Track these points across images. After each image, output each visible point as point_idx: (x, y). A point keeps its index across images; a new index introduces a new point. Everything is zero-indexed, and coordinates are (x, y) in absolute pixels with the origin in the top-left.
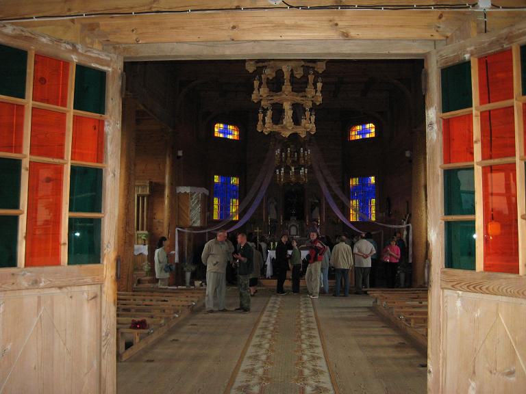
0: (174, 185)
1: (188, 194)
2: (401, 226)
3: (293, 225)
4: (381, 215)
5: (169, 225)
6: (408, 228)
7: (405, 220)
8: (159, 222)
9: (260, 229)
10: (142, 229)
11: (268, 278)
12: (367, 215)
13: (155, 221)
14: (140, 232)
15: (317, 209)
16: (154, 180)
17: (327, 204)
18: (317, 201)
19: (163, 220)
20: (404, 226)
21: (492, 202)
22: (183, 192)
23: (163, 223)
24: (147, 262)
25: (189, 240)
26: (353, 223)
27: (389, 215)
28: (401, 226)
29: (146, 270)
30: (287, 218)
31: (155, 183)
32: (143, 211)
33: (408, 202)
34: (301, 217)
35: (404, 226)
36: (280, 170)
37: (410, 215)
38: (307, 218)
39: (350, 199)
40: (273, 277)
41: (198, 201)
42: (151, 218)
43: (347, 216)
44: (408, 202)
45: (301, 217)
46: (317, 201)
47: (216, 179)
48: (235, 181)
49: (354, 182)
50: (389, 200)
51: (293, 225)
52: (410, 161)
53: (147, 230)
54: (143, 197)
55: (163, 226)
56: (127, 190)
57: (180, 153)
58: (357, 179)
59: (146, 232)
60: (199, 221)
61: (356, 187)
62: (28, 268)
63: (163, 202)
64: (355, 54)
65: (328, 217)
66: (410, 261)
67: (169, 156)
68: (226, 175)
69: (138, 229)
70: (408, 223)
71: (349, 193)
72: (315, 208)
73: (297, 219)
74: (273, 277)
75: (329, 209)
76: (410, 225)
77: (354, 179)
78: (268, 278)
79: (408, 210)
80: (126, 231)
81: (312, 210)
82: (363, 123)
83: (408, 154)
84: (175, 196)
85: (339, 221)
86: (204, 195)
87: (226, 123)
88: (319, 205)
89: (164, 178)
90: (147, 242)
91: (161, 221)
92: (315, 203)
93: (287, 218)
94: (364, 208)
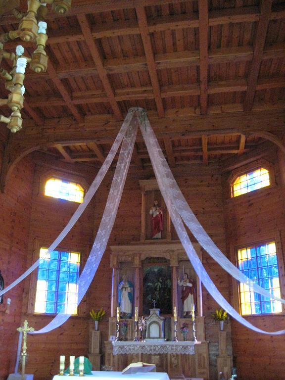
15: (191, 297)
17: (204, 289)
18: (191, 285)
26: (246, 317)
36: (92, 312)
38: (175, 310)
40: (172, 267)
43: (236, 305)
46: (191, 285)
62: (161, 100)
64: (140, 283)
65: (209, 309)
72: (187, 296)
73: (160, 313)
74: (172, 267)
75: (207, 297)
81: (183, 298)
82: (256, 244)
85: (225, 314)
88: (193, 290)
92: (187, 287)
93: (144, 313)
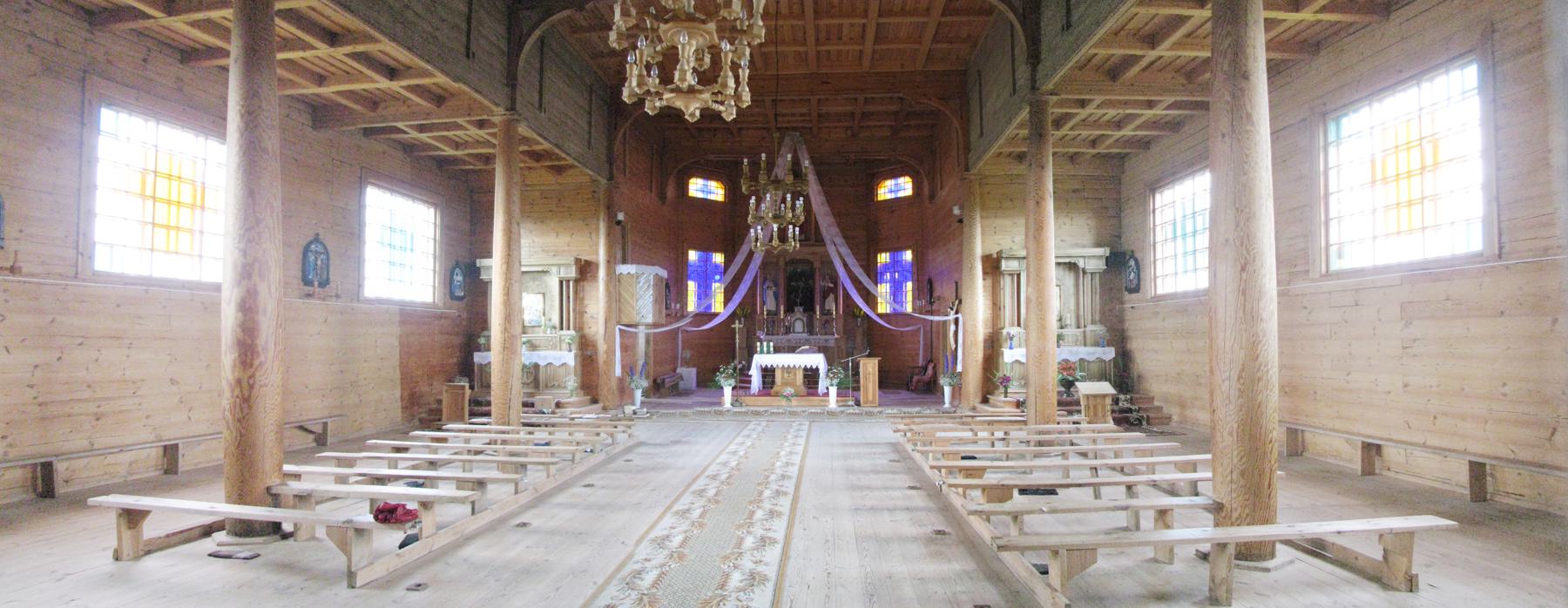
0: (611, 262)
1: (633, 275)
2: (946, 318)
3: (797, 319)
4: (918, 303)
5: (607, 321)
6: (956, 321)
7: (952, 309)
8: (592, 317)
9: (740, 323)
10: (569, 329)
11: (754, 395)
12: (901, 303)
13: (586, 316)
14: (565, 332)
15: (832, 296)
16: (584, 257)
17: (844, 289)
18: (832, 285)
19: (598, 314)
20: (952, 317)
21: (302, 445)
22: (625, 273)
23: (597, 319)
24: (573, 376)
25: (648, 342)
26: (880, 316)
27: (931, 303)
28: (946, 318)
29: (569, 388)
30: (789, 310)
31: (586, 261)
32: (569, 302)
33: (957, 283)
34: (809, 308)
35: (952, 317)
37: (960, 302)
38: (818, 308)
39: (876, 281)
41: (649, 286)
42: (580, 313)
44: (957, 283)
45: (809, 308)
46: (832, 285)
47: (693, 255)
48: (718, 258)
49: (883, 258)
50: (930, 282)
51: (797, 319)
52: (961, 221)
53: (575, 329)
54: (568, 281)
55: (597, 323)
56: (505, 266)
57: (621, 217)
58: (888, 254)
59: (572, 332)
60: (651, 316)
61: (885, 266)
63: (598, 289)
66: (959, 369)
67: (604, 220)
68: (706, 248)
69: (562, 329)
70: (957, 313)
71: (874, 274)
72: (828, 295)
75: (847, 296)
76: (959, 315)
77: (883, 255)
78: (754, 395)
79: (957, 293)
80: (506, 329)
81: (825, 297)
83: (956, 211)
84: (614, 280)
86: (657, 277)
87: (707, 177)
88: (834, 290)
89: (597, 253)
90: (573, 347)
91: (595, 316)
93: (789, 310)
94: (704, 293)
